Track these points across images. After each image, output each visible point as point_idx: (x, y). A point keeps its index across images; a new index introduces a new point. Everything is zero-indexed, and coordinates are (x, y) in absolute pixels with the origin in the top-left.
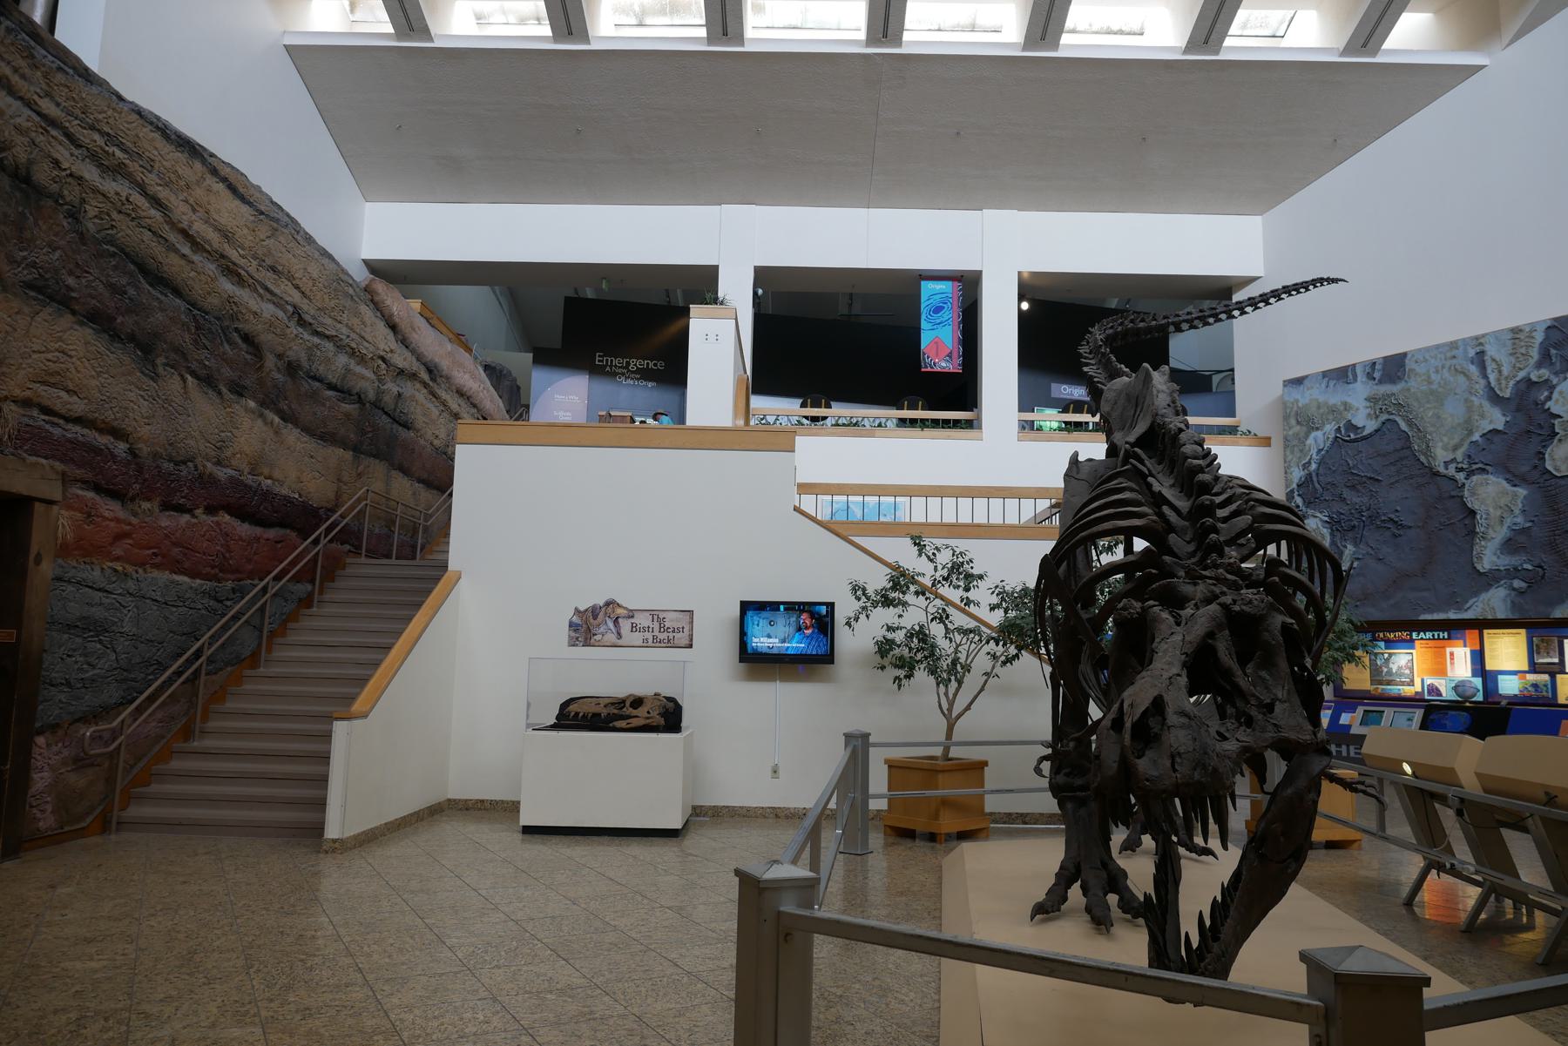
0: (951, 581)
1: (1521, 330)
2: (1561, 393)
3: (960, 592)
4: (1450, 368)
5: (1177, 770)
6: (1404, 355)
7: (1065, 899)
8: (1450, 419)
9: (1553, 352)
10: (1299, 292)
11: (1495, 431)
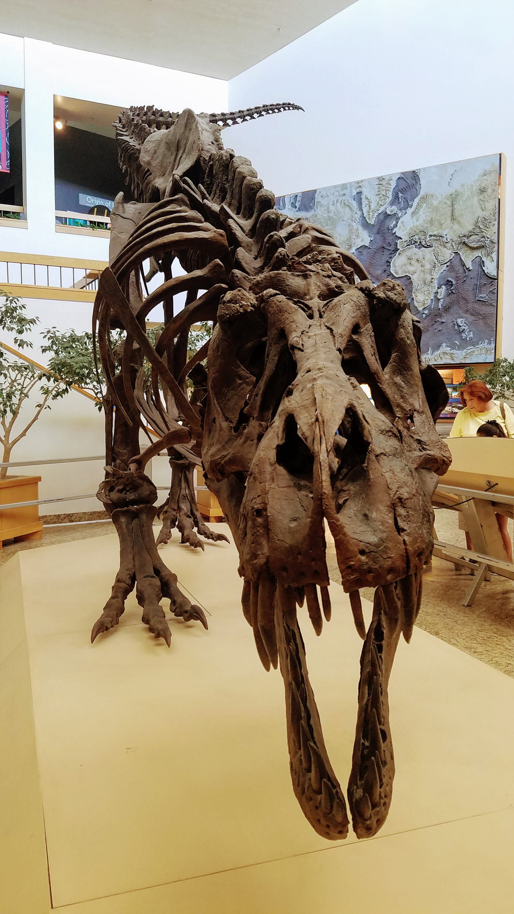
0: (5, 324)
1: (383, 179)
2: (402, 222)
3: (14, 334)
4: (341, 202)
5: (403, 530)
6: (315, 191)
7: (122, 610)
8: (339, 237)
9: (400, 195)
10: (274, 112)
11: (364, 247)
